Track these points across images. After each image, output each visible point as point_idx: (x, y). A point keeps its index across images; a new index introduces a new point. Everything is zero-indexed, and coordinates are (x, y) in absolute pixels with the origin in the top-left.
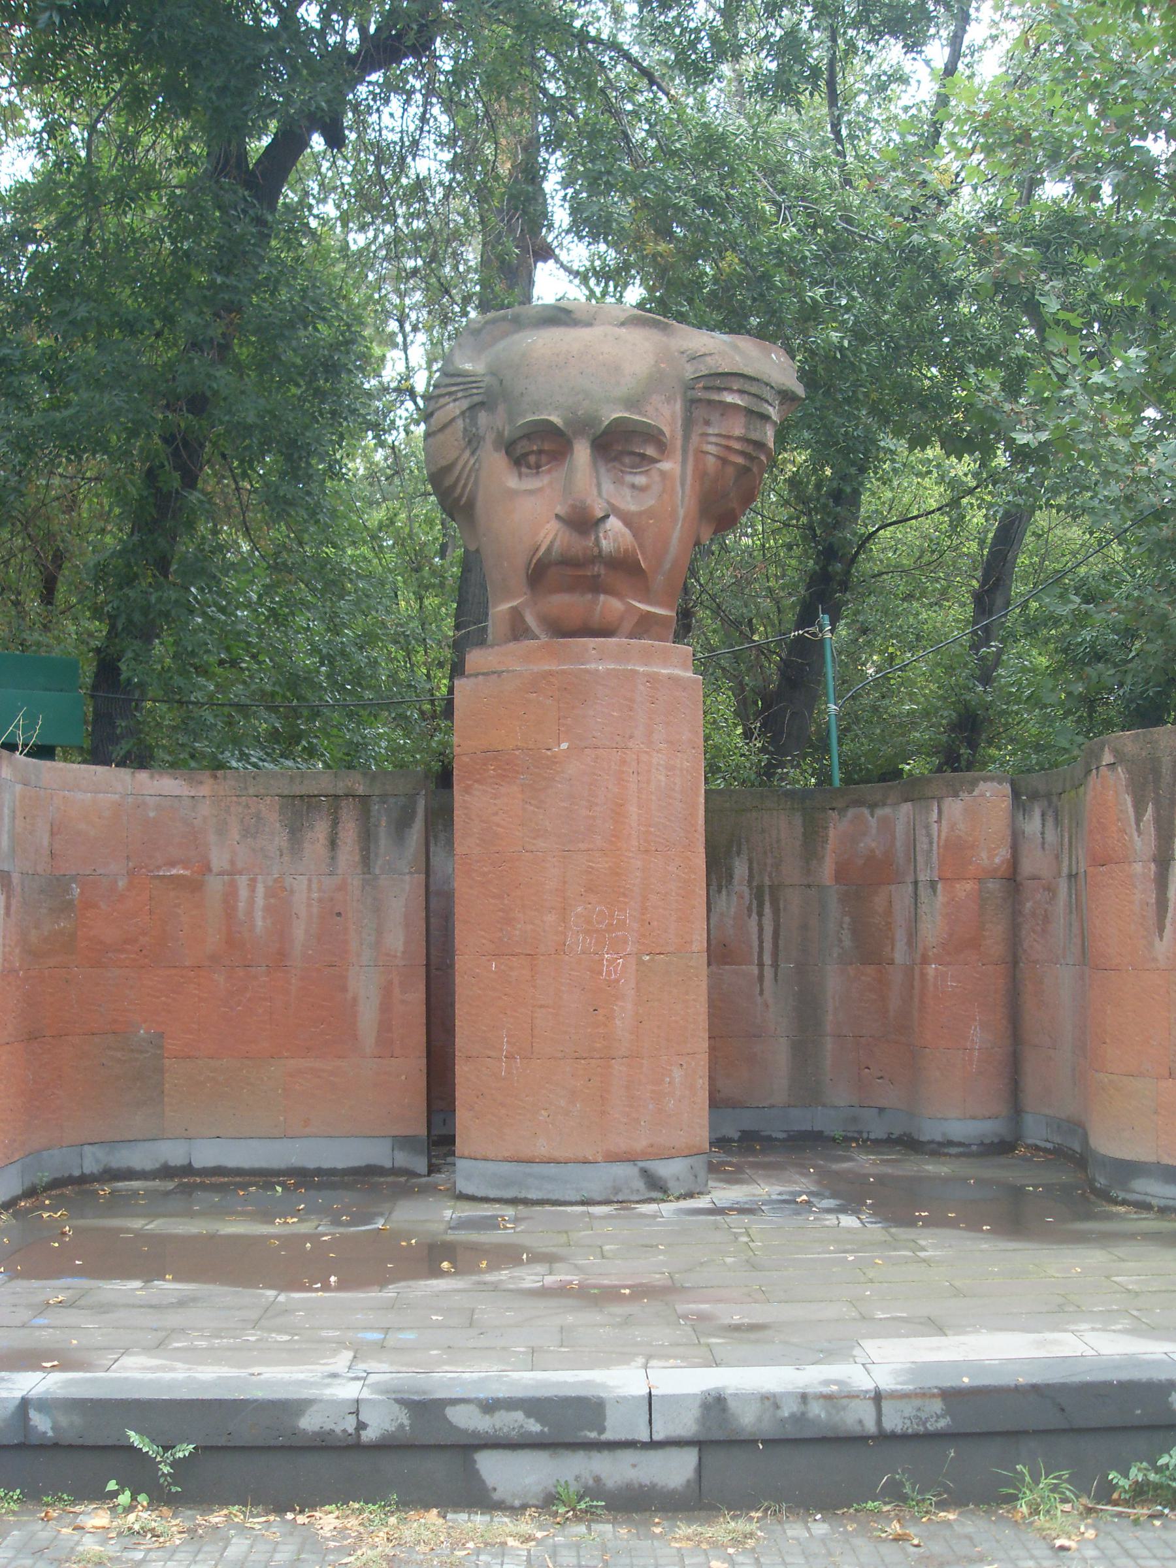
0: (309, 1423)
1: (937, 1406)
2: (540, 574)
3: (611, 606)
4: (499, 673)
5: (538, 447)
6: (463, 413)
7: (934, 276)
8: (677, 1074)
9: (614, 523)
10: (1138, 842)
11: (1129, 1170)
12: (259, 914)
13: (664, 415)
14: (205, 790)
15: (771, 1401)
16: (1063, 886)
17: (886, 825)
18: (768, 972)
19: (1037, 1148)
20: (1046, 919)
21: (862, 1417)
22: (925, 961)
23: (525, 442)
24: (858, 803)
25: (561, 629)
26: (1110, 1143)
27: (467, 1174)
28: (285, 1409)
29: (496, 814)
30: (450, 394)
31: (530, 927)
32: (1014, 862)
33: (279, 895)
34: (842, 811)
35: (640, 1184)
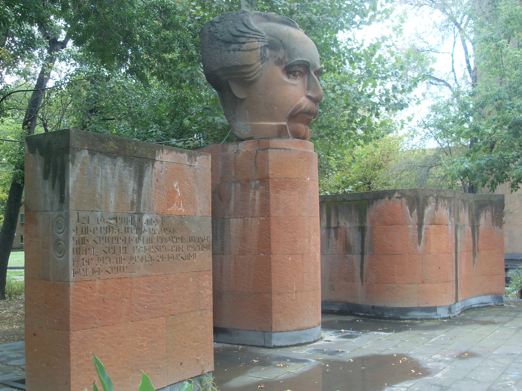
6: (261, 47)
10: (411, 219)
23: (297, 67)
29: (290, 202)
30: (256, 38)
31: (302, 244)
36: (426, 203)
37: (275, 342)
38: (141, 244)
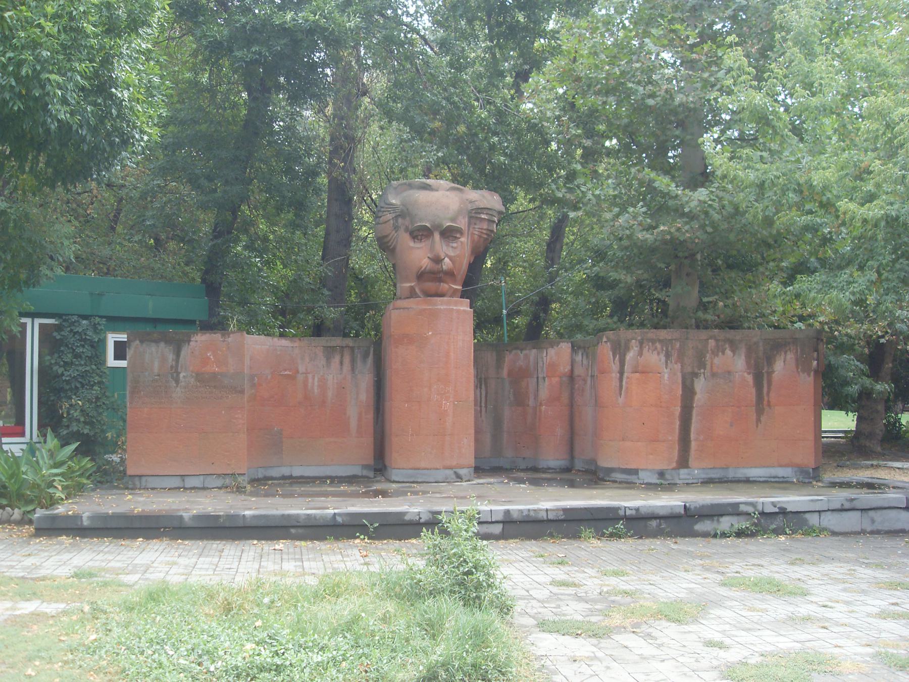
0: (407, 518)
1: (562, 513)
2: (421, 276)
3: (444, 286)
4: (408, 309)
5: (421, 233)
7: (542, 136)
8: (465, 440)
9: (447, 260)
11: (611, 470)
12: (316, 388)
13: (462, 223)
14: (296, 344)
15: (521, 511)
16: (589, 379)
17: (527, 357)
18: (483, 409)
19: (579, 471)
20: (583, 390)
21: (543, 515)
22: (541, 405)
24: (517, 348)
25: (428, 294)
26: (604, 463)
27: (395, 475)
28: (402, 514)
32: (572, 371)
33: (323, 381)
34: (510, 352)
35: (454, 476)
36: (627, 348)
37: (394, 478)
38: (178, 389)
